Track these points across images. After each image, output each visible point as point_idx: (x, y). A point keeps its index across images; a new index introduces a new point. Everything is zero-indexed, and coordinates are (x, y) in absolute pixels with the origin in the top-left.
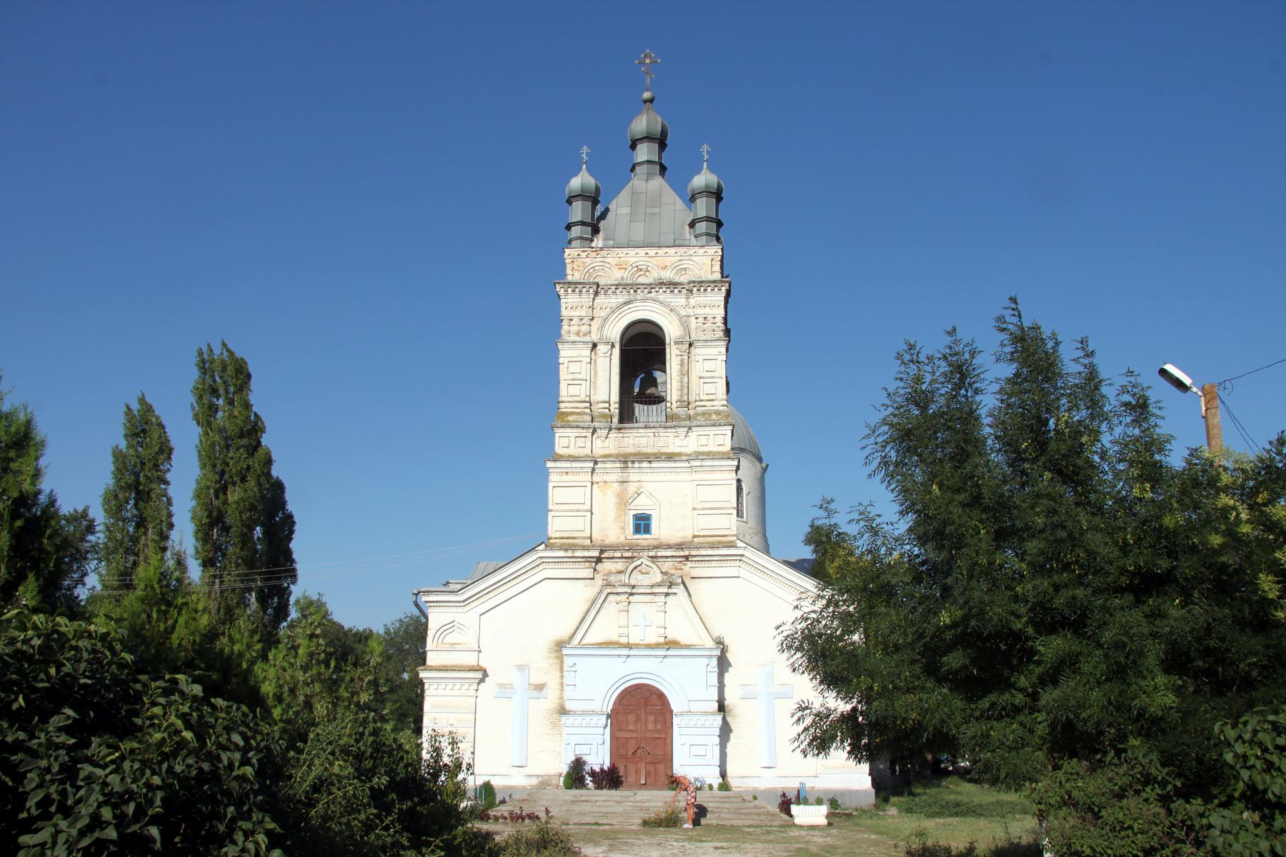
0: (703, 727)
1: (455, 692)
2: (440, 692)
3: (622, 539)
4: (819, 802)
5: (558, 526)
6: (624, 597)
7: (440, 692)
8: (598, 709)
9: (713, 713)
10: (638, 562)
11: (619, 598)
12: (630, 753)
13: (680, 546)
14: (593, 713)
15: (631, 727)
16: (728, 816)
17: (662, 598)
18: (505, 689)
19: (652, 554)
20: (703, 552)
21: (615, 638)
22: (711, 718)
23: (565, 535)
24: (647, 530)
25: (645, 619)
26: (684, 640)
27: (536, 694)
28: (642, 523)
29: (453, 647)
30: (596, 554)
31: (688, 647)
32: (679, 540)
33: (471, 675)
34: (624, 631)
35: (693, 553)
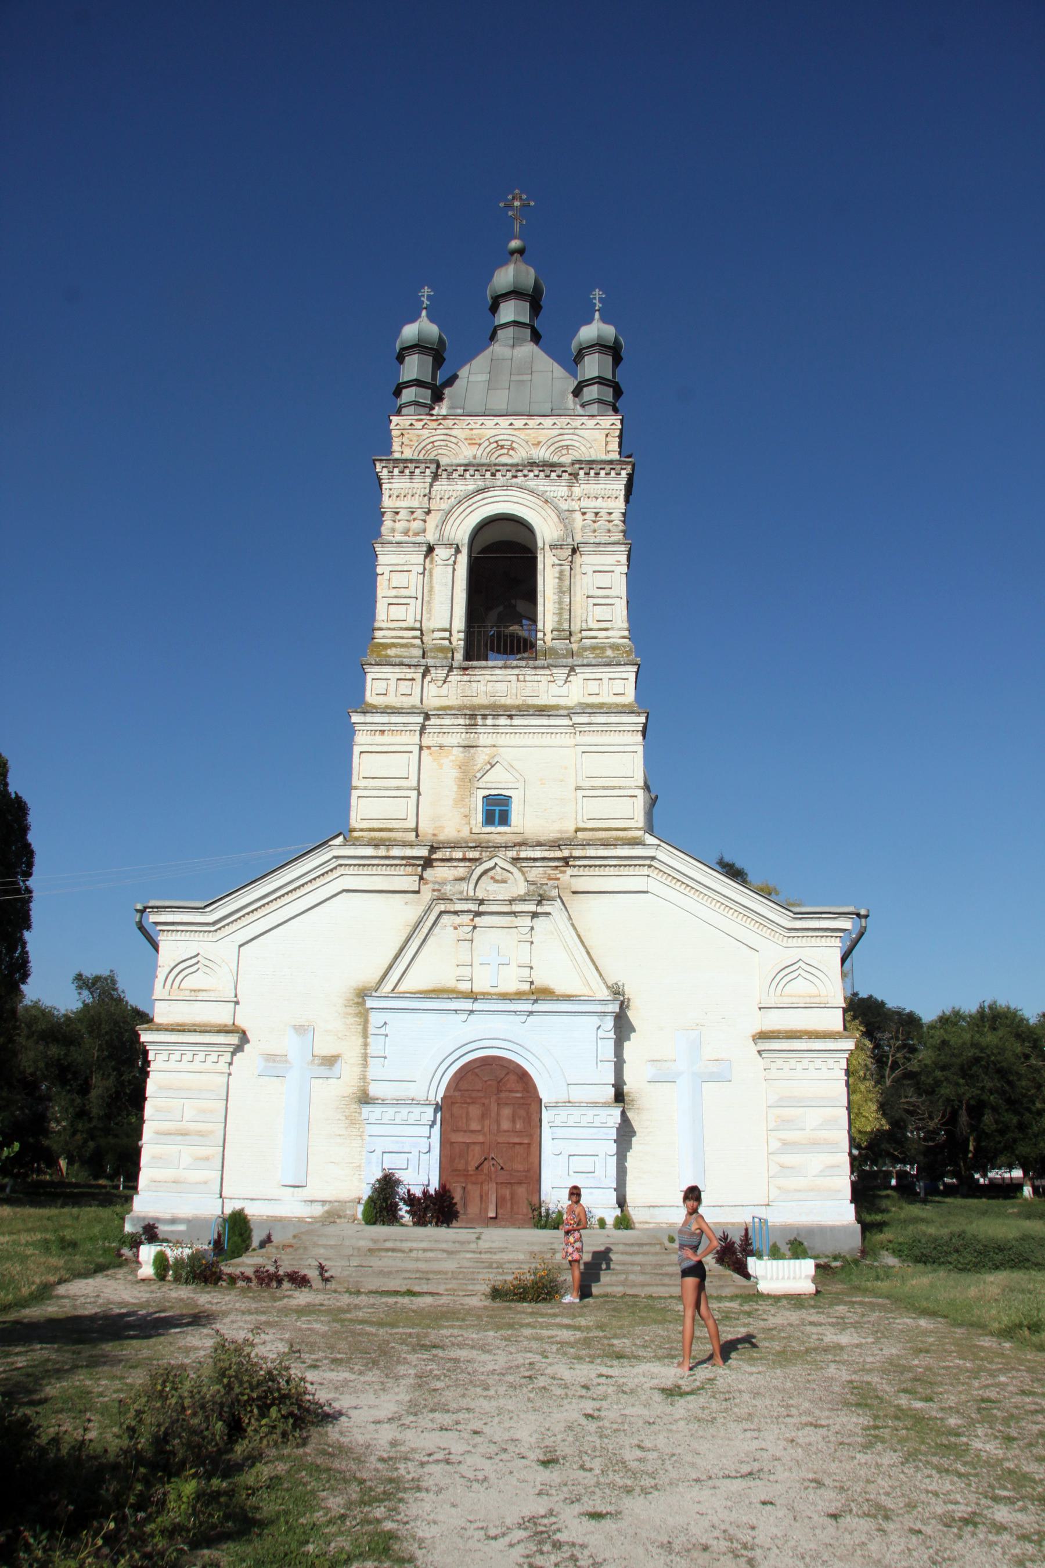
0: (590, 1126)
1: (196, 1066)
2: (172, 1065)
3: (465, 833)
5: (364, 811)
6: (466, 919)
7: (172, 1065)
8: (421, 1096)
9: (606, 1105)
11: (457, 920)
12: (471, 1168)
13: (556, 845)
14: (413, 1102)
15: (475, 1126)
16: (642, 1278)
17: (527, 921)
20: (591, 852)
21: (450, 983)
22: (603, 1112)
25: (499, 955)
27: (323, 1071)
28: (497, 810)
29: (196, 996)
30: (424, 852)
31: (568, 998)
33: (221, 1039)
34: (466, 971)
35: (577, 853)
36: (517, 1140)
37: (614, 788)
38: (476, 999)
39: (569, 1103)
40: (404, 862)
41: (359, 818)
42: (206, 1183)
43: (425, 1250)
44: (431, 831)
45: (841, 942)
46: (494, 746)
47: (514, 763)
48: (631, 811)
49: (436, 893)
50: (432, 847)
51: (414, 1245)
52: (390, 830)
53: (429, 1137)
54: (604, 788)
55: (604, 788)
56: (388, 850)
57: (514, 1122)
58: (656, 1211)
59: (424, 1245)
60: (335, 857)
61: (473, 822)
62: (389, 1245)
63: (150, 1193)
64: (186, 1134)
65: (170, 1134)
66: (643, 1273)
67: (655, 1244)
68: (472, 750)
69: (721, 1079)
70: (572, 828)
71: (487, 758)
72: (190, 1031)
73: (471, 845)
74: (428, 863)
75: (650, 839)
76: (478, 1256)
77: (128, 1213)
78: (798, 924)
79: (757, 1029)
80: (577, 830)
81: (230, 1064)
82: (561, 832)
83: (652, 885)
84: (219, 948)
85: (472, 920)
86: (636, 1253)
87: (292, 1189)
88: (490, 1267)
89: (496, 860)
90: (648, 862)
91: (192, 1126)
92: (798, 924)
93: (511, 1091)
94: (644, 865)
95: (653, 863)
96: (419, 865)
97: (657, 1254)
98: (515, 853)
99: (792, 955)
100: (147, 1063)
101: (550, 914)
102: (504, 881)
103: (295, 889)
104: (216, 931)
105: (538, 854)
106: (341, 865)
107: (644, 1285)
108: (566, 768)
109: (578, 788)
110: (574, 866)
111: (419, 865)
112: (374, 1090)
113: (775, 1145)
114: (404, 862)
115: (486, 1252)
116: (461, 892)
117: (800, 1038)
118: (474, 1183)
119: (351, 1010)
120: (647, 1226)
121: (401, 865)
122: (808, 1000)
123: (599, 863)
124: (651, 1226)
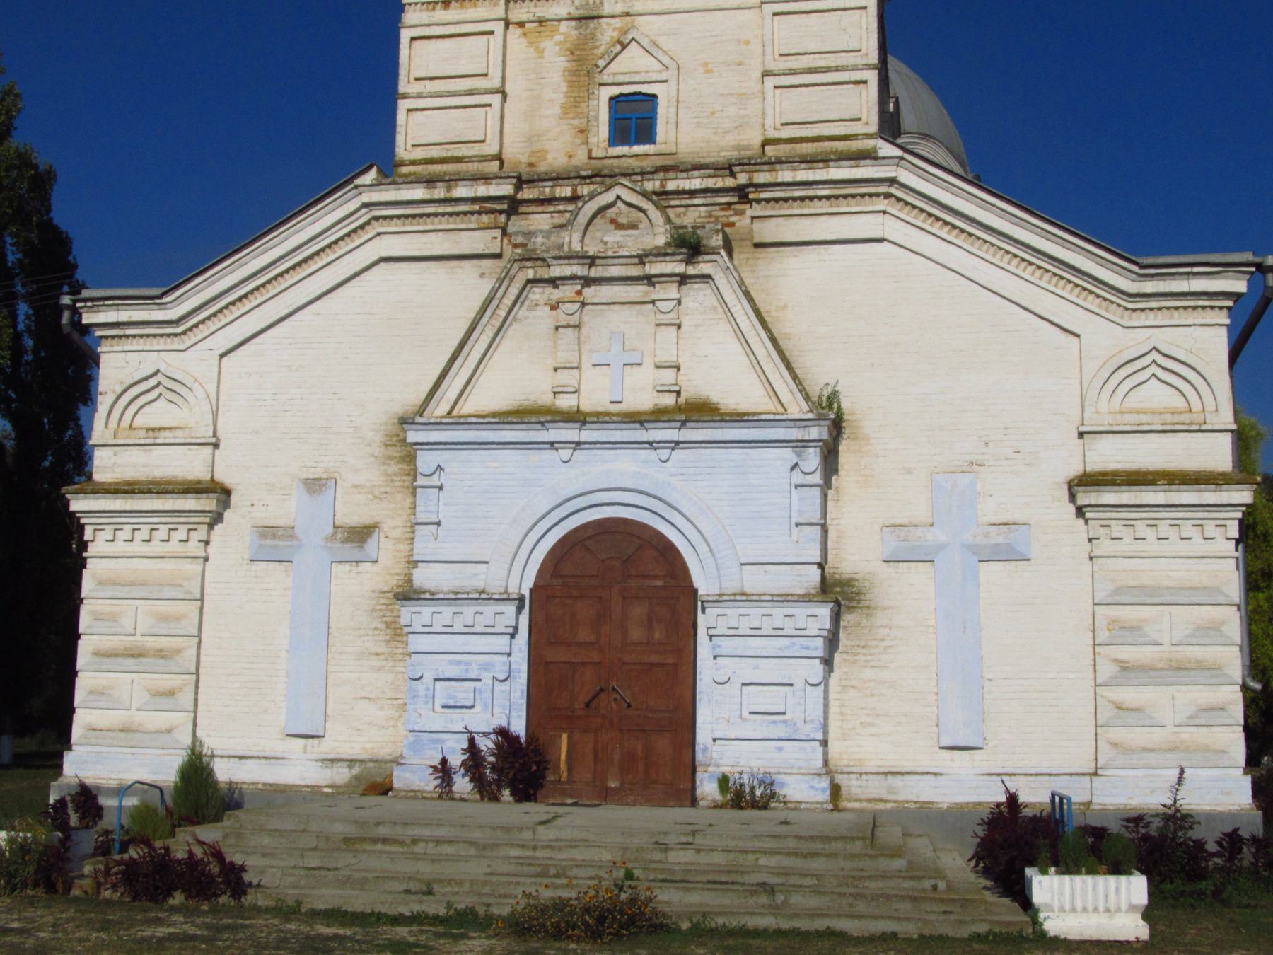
0: (778, 633)
1: (156, 547)
2: (119, 547)
3: (581, 157)
4: (441, 172)
5: (418, 129)
6: (567, 291)
7: (119, 547)
8: (496, 587)
9: (806, 598)
10: (609, 197)
11: (556, 294)
12: (579, 706)
13: (729, 168)
14: (483, 596)
15: (585, 635)
16: (814, 902)
17: (672, 291)
18: (275, 541)
19: (650, 186)
20: (785, 175)
21: (545, 399)
22: (801, 611)
23: (435, 153)
24: (645, 132)
25: (628, 349)
26: (729, 400)
27: (349, 551)
28: (634, 116)
29: (154, 437)
30: (506, 189)
31: (739, 418)
32: (725, 156)
33: (190, 503)
34: (566, 378)
35: (761, 178)
36: (654, 659)
37: (828, 70)
38: (584, 423)
39: (744, 597)
40: (476, 207)
41: (410, 143)
42: (169, 731)
43: (438, 842)
44: (524, 159)
45: (1230, 317)
46: (628, 14)
47: (661, 41)
48: (859, 106)
49: (519, 251)
50: (519, 178)
51: (426, 832)
52: (458, 160)
53: (509, 655)
54: (810, 71)
55: (810, 71)
56: (449, 189)
57: (650, 627)
58: (897, 782)
59: (442, 832)
60: (365, 205)
61: (593, 140)
62: (383, 831)
63: (89, 748)
64: (140, 655)
65: (117, 655)
66: (816, 891)
67: (852, 839)
68: (592, 24)
69: (1012, 556)
70: (757, 140)
71: (615, 34)
72: (142, 492)
73: (584, 173)
74: (514, 206)
75: (886, 149)
76: (530, 853)
77: (55, 780)
78: (1149, 286)
79: (1075, 469)
80: (766, 142)
81: (207, 543)
82: (739, 148)
83: (891, 228)
84: (191, 361)
85: (579, 293)
86: (814, 855)
87: (302, 741)
88: (544, 874)
89: (618, 190)
90: (883, 189)
91: (151, 642)
92: (1149, 286)
93: (645, 577)
94: (878, 195)
95: (893, 190)
96: (501, 212)
97: (853, 856)
98: (657, 183)
99: (1138, 341)
100: (84, 546)
101: (709, 276)
102: (633, 226)
103: (305, 261)
104: (184, 333)
105: (696, 184)
106: (377, 218)
107: (814, 914)
108: (747, 43)
109: (766, 74)
110: (758, 201)
111: (501, 212)
112: (424, 577)
113: (1107, 670)
114: (476, 207)
115: (543, 847)
116: (561, 247)
117: (1152, 483)
118: (585, 731)
119: (393, 452)
120: (881, 806)
121: (472, 213)
122: (1168, 418)
123: (800, 197)
124: (889, 806)
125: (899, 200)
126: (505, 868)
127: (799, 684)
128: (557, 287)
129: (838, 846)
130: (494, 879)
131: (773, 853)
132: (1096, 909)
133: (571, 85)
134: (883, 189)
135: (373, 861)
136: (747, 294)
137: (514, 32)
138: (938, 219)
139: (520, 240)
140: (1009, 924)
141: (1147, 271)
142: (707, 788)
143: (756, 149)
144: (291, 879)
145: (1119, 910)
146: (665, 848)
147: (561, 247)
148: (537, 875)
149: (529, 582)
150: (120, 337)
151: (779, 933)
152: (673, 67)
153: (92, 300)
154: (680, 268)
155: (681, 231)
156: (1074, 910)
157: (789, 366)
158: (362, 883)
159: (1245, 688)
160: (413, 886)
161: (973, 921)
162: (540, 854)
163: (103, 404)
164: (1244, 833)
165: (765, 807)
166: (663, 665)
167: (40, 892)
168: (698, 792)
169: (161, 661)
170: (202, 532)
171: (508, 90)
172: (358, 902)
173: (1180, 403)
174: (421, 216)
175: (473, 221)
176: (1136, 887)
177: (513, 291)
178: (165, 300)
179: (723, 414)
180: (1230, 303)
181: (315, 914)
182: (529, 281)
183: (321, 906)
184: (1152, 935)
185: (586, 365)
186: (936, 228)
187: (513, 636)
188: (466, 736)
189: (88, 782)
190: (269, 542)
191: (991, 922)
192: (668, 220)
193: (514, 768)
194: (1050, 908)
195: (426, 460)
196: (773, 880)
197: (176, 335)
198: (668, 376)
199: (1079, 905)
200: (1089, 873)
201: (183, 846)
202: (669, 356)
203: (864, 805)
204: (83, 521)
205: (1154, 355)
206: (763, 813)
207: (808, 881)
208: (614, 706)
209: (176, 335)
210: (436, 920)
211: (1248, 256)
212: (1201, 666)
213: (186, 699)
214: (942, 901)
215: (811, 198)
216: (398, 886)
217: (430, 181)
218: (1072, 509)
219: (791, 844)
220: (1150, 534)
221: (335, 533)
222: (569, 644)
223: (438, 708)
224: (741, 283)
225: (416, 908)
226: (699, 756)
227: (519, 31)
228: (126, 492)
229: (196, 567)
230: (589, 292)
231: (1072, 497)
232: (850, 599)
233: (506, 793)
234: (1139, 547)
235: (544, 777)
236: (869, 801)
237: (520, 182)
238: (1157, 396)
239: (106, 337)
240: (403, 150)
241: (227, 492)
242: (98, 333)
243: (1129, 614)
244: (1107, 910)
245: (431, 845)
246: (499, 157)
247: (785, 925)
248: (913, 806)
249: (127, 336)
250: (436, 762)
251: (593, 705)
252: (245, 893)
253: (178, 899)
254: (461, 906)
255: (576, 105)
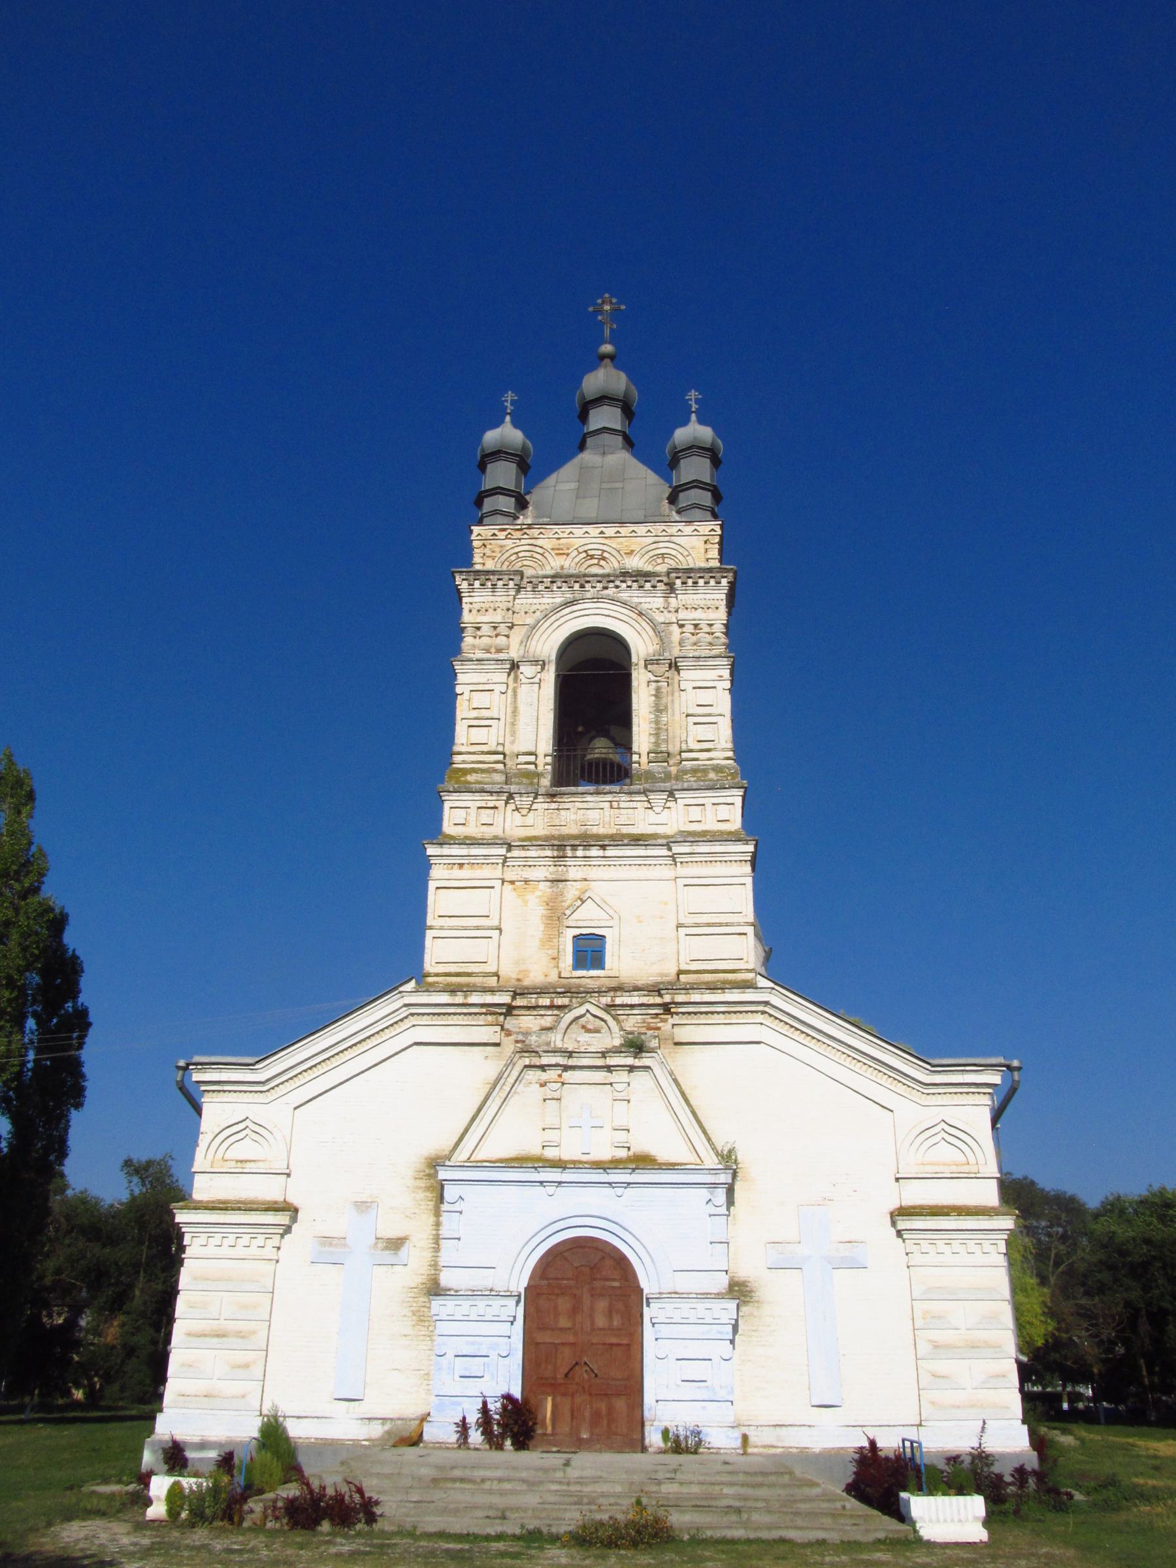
1: (239, 1252)
2: (211, 1251)
3: (553, 977)
4: (459, 985)
5: (440, 952)
6: (552, 1074)
8: (500, 1287)
9: (719, 1296)
11: (544, 1076)
12: (560, 1376)
13: (656, 990)
14: (492, 1293)
15: (564, 1322)
17: (623, 1076)
20: (696, 997)
21: (536, 1150)
25: (595, 1115)
26: (662, 1156)
27: (388, 1256)
28: (589, 951)
30: (505, 999)
31: (672, 1167)
33: (269, 1218)
34: (551, 1135)
35: (680, 998)
36: (614, 1340)
37: (720, 925)
38: (565, 1168)
39: (675, 1295)
40: (484, 1010)
42: (243, 1396)
43: (500, 1480)
44: (514, 976)
54: (709, 925)
55: (709, 925)
60: (405, 1005)
61: (562, 965)
62: (457, 1473)
63: (177, 1410)
65: (205, 1335)
66: (769, 1511)
68: (561, 885)
70: (673, 971)
71: (577, 893)
73: (559, 990)
74: (510, 1010)
75: (763, 982)
76: (565, 1488)
78: (938, 1079)
80: (680, 972)
84: (269, 1111)
85: (560, 1076)
86: (761, 1485)
89: (587, 1006)
90: (761, 1008)
91: (232, 1326)
92: (938, 1079)
94: (756, 1012)
95: (766, 1009)
96: (501, 1014)
99: (932, 1115)
100: (182, 1248)
101: (649, 1067)
102: (597, 1031)
105: (635, 1000)
106: (412, 1015)
107: (770, 1528)
108: (666, 904)
109: (679, 926)
110: (677, 1014)
111: (501, 1014)
114: (484, 1010)
116: (548, 1044)
120: (773, 1451)
121: (481, 1014)
122: (954, 1169)
125: (771, 1015)
126: (552, 1499)
127: (716, 1359)
128: (544, 1071)
129: (773, 1478)
130: (547, 1506)
131: (732, 1484)
132: (952, 1521)
133: (547, 925)
134: (761, 1008)
135: (459, 1495)
136: (675, 1081)
137: (507, 886)
138: (797, 1029)
139: (520, 1037)
140: (899, 1531)
141: (936, 1068)
142: (654, 1438)
143: (672, 977)
144: (404, 1510)
145: (967, 1520)
146: (659, 1483)
147: (548, 1044)
148: (575, 1504)
149: (524, 1283)
150: (219, 1091)
151: (749, 1541)
152: (616, 917)
153: (201, 1064)
154: (630, 1061)
155: (630, 1036)
156: (938, 1521)
157: (704, 1132)
158: (456, 1512)
159: (1018, 1361)
160: (491, 1513)
161: (876, 1530)
162: (573, 1488)
163: (203, 1141)
164: (1028, 1468)
165: (696, 1452)
166: (619, 1345)
167: (226, 1523)
168: (647, 1442)
169: (240, 1340)
170: (276, 1240)
171: (503, 927)
172: (457, 1526)
173: (960, 1158)
174: (444, 1014)
175: (481, 1020)
176: (976, 1505)
177: (515, 1074)
178: (257, 1067)
179: (660, 1164)
180: (990, 1091)
181: (429, 1536)
182: (526, 1066)
183: (431, 1529)
184: (989, 1538)
185: (565, 1127)
186: (796, 1035)
187: (512, 1323)
188: (480, 1400)
189: (178, 1438)
190: (327, 1249)
191: (888, 1531)
192: (622, 1029)
193: (514, 1424)
194: (922, 1519)
195: (450, 1192)
196: (737, 1504)
197: (261, 1092)
198: (622, 1136)
199: (941, 1519)
200: (944, 1494)
201: (276, 1487)
202: (621, 1122)
203: (761, 1450)
204: (183, 1230)
205: (943, 1125)
206: (691, 1457)
207: (761, 1504)
208: (586, 1376)
209: (261, 1092)
210: (516, 1538)
211: (1001, 1060)
212: (988, 1345)
213: (257, 1371)
214: (852, 1516)
215: (712, 1013)
216: (481, 1513)
217: (453, 990)
218: (893, 1231)
219: (741, 1477)
220: (947, 1249)
221: (376, 1244)
222: (553, 1330)
223: (457, 1378)
224: (671, 1073)
225: (499, 1529)
226: (647, 1414)
227: (511, 886)
228: (221, 1209)
229: (270, 1266)
230: (567, 1076)
231: (894, 1224)
232: (745, 1296)
233: (508, 1443)
234: (941, 1258)
235: (534, 1431)
236: (765, 1447)
237: (515, 995)
238: (946, 1155)
239: (208, 1091)
240: (429, 966)
241: (296, 1210)
242: (203, 1088)
243: (937, 1307)
244: (960, 1521)
245: (495, 1483)
246: (497, 975)
247: (752, 1535)
248: (795, 1450)
249: (224, 1091)
250: (458, 1419)
251: (570, 1376)
252: (376, 1521)
253: (325, 1526)
254: (531, 1527)
255: (550, 940)
